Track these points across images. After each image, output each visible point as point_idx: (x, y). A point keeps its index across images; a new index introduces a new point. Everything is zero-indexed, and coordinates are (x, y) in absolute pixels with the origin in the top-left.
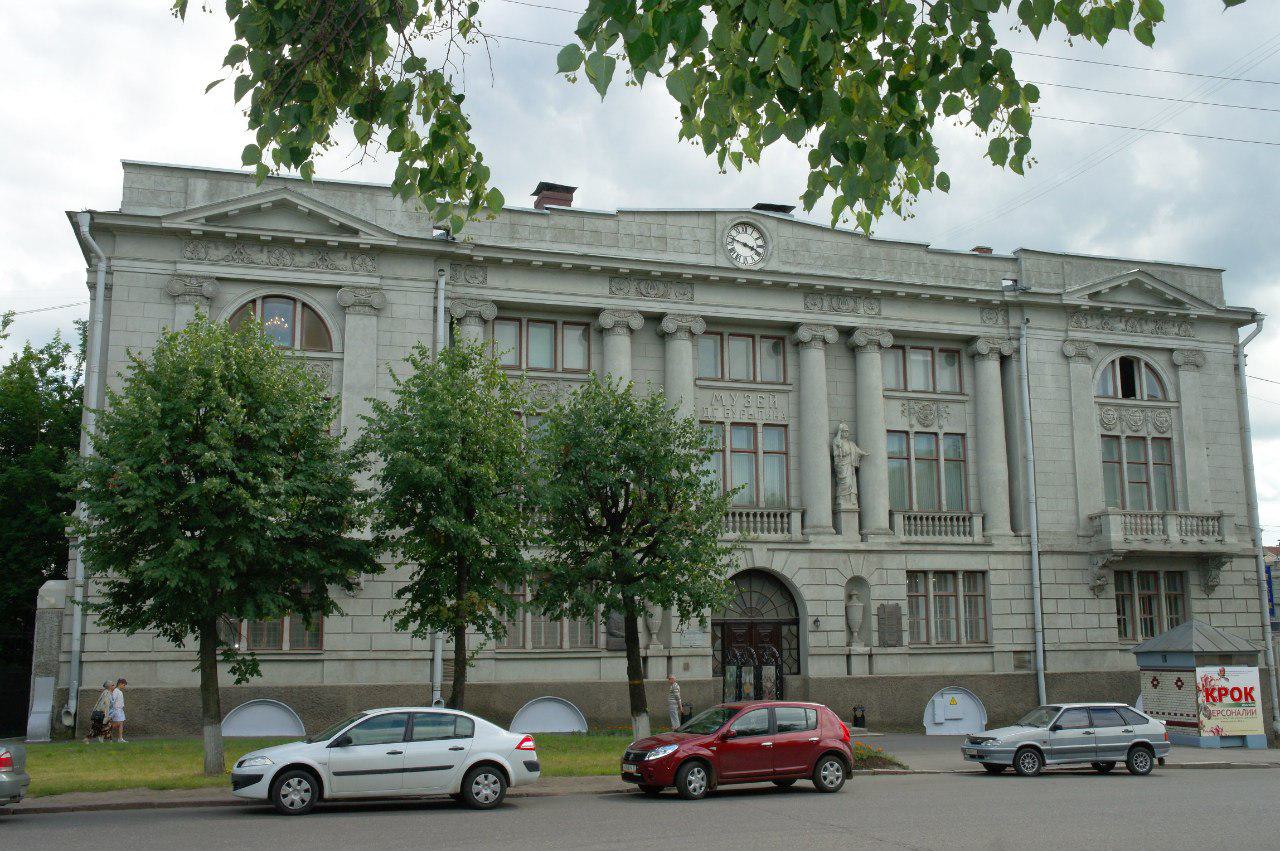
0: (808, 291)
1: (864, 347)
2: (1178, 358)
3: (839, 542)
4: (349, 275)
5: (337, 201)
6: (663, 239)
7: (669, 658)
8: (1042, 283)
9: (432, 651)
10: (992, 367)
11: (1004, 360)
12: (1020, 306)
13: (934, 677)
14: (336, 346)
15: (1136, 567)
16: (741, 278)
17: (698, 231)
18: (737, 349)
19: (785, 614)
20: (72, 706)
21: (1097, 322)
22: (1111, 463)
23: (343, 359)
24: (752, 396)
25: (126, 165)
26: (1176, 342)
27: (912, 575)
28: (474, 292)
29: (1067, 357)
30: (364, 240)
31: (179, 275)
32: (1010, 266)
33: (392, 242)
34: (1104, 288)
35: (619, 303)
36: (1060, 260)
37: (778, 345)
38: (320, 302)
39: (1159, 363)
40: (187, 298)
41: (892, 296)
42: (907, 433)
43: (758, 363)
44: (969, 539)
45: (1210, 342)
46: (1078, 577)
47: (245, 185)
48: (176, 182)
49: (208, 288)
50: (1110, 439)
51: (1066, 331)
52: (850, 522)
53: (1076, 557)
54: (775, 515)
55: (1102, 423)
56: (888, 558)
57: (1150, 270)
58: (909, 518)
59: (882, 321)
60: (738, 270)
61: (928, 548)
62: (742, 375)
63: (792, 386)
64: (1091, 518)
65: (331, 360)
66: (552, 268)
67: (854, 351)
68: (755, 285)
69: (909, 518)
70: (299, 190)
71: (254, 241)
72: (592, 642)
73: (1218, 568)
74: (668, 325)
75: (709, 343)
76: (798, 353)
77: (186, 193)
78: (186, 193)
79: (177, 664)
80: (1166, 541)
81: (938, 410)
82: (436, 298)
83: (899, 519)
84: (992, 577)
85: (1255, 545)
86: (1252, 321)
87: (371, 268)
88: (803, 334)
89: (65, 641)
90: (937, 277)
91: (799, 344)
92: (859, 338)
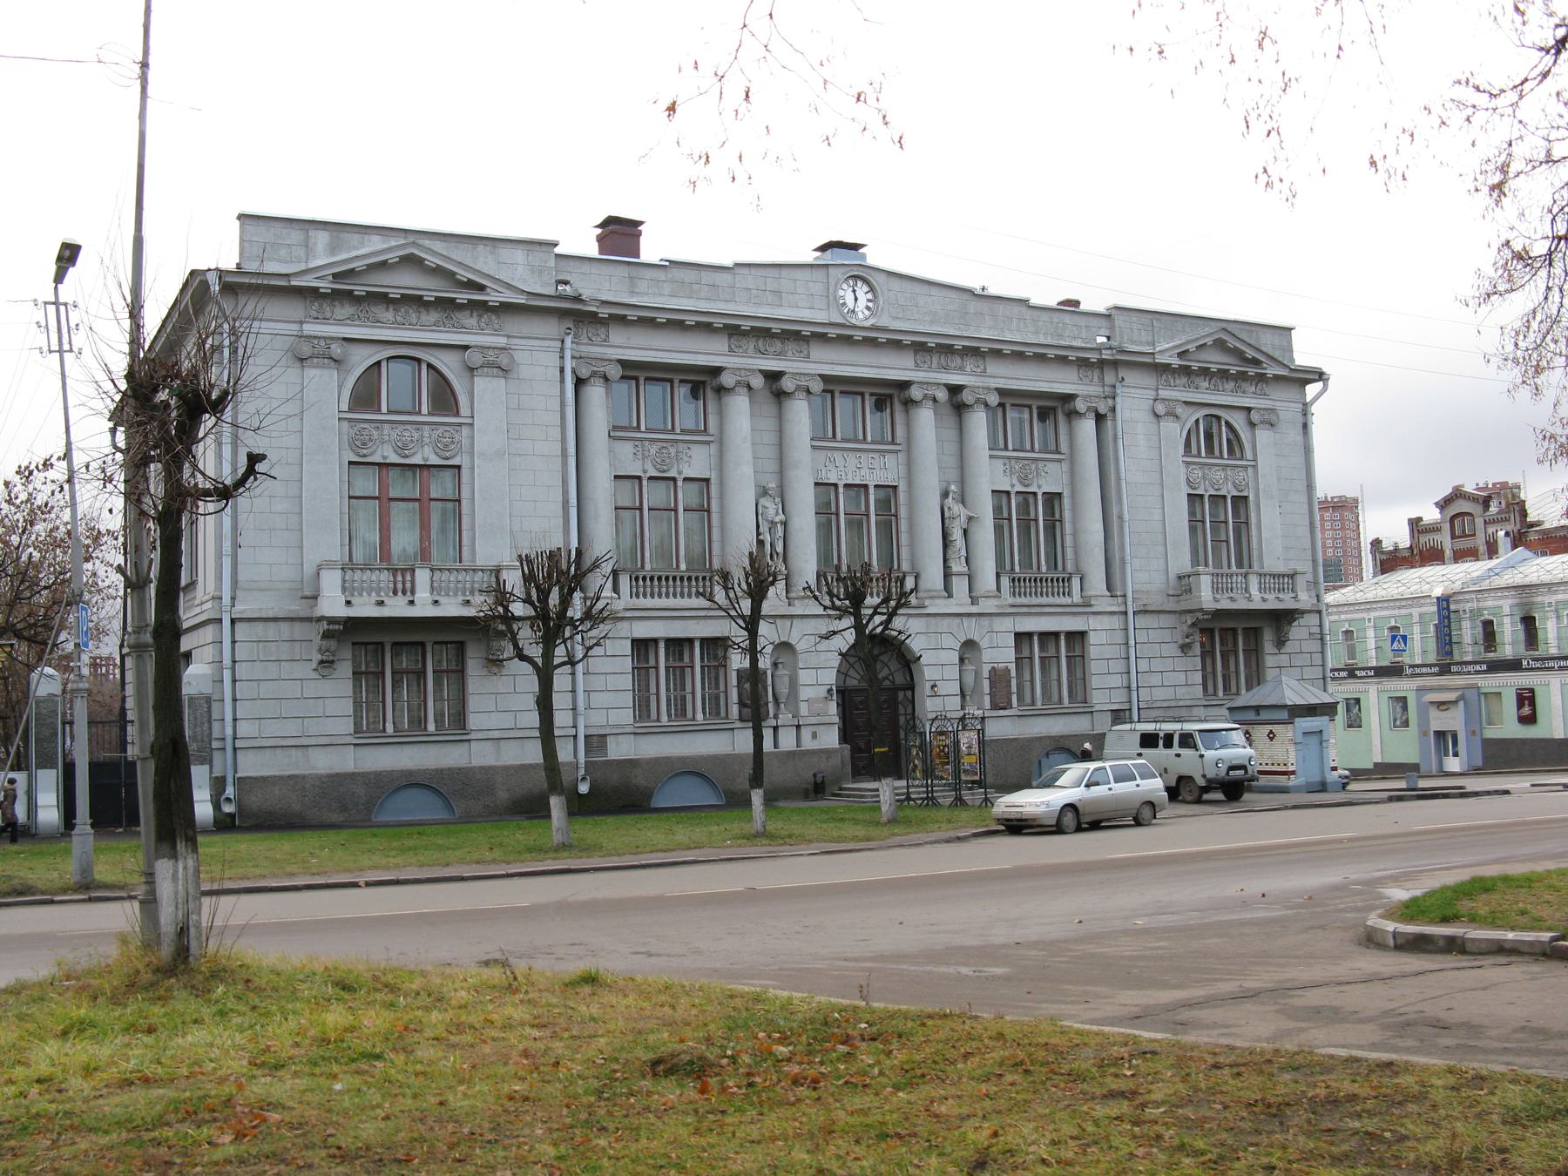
0: (919, 348)
1: (972, 406)
2: (1255, 416)
3: (951, 607)
4: (478, 335)
5: (459, 253)
6: (778, 293)
7: (798, 727)
8: (1135, 342)
9: (575, 727)
10: (1087, 426)
11: (1100, 418)
12: (1115, 364)
13: (1040, 738)
14: (465, 410)
15: (1217, 625)
16: (858, 335)
17: (811, 284)
18: (654, 393)
19: (900, 679)
20: (230, 791)
21: (1184, 380)
22: (1195, 524)
23: (472, 425)
24: (864, 456)
25: (241, 217)
26: (1254, 401)
27: (1022, 638)
28: (596, 350)
29: (1157, 416)
30: (493, 298)
31: (307, 337)
32: (1104, 322)
33: (521, 300)
34: (1192, 347)
35: (927, 376)
36: (1150, 316)
37: (696, 390)
38: (448, 364)
39: (1238, 421)
40: (315, 360)
41: (622, 320)
42: (639, 478)
43: (677, 409)
44: (1067, 600)
45: (1280, 400)
46: (1167, 636)
47: (366, 237)
48: (296, 236)
49: (336, 350)
50: (1194, 499)
51: (1157, 389)
52: (960, 586)
53: (1166, 616)
54: (667, 579)
55: (1189, 482)
56: (997, 621)
57: (1230, 327)
58: (637, 579)
59: (987, 380)
60: (854, 327)
61: (1034, 610)
62: (690, 425)
63: (710, 435)
64: (1180, 578)
65: (460, 425)
66: (677, 325)
67: (780, 396)
68: (870, 342)
69: (637, 579)
70: (421, 242)
71: (383, 299)
72: (419, 723)
73: (1290, 623)
74: (967, 397)
75: (623, 389)
76: (907, 411)
77: (307, 246)
78: (307, 245)
79: (329, 749)
80: (1249, 599)
81: (1037, 468)
82: (562, 358)
83: (1005, 581)
84: (1093, 638)
85: (1318, 601)
86: (1320, 379)
87: (497, 327)
88: (727, 380)
89: (216, 726)
90: (1037, 333)
91: (721, 390)
92: (787, 384)
